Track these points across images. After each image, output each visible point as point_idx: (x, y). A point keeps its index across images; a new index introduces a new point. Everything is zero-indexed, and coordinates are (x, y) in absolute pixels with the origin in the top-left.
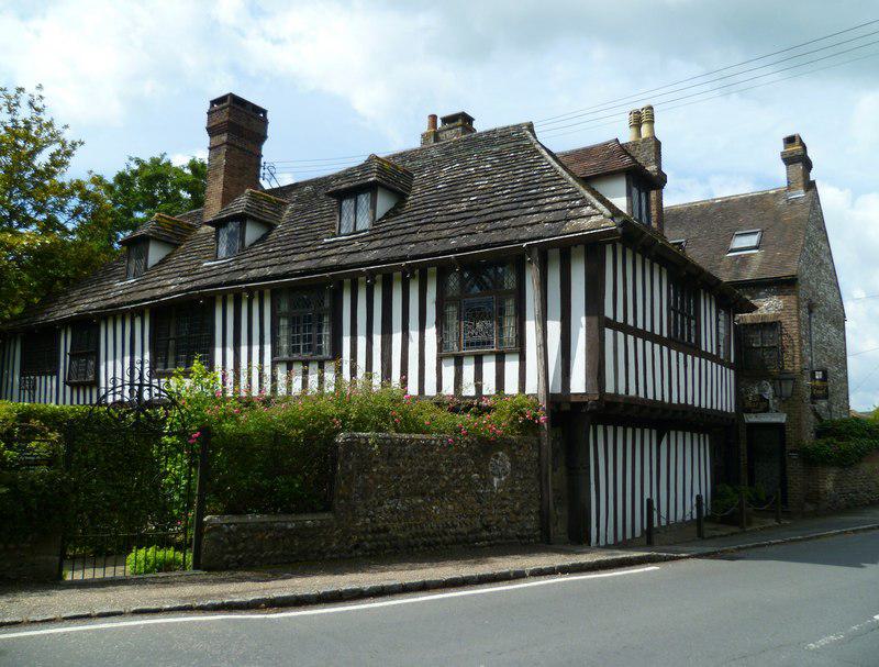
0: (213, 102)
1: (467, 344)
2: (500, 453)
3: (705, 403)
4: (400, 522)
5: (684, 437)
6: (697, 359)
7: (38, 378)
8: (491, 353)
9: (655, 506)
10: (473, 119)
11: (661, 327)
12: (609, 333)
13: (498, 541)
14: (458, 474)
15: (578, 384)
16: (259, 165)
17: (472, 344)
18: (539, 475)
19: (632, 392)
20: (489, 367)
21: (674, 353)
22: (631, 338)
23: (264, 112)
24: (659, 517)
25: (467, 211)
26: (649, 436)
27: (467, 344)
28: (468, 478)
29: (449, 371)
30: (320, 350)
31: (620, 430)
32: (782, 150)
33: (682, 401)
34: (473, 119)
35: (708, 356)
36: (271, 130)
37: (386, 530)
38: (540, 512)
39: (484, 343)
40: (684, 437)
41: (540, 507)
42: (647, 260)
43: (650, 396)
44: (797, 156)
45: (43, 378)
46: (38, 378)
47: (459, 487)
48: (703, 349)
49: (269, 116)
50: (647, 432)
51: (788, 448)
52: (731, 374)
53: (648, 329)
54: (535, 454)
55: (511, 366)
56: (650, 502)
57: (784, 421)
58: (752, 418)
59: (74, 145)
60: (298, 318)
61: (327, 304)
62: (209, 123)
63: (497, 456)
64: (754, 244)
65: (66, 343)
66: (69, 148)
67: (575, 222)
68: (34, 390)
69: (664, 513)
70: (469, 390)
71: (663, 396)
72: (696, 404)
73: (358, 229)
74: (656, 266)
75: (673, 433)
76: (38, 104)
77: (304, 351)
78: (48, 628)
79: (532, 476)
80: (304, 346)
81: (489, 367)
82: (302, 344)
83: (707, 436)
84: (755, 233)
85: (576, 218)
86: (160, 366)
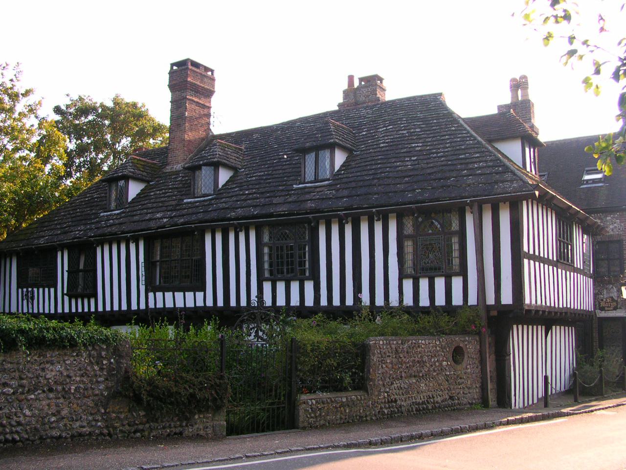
0: (173, 65)
3: (578, 306)
6: (537, 264)
7: (35, 290)
8: (441, 276)
9: (550, 381)
10: (383, 79)
11: (553, 256)
13: (458, 407)
14: (435, 362)
15: (507, 298)
19: (539, 302)
20: (440, 283)
22: (532, 262)
23: (212, 71)
24: (552, 387)
25: (412, 170)
26: (541, 330)
28: (441, 365)
29: (408, 284)
34: (383, 79)
35: (576, 270)
37: (396, 401)
39: (435, 269)
40: (542, 328)
42: (549, 209)
44: (554, 9)
45: (41, 290)
46: (35, 290)
48: (576, 266)
49: (216, 75)
50: (539, 327)
52: (591, 281)
53: (531, 252)
55: (457, 283)
56: (546, 378)
58: (603, 314)
60: (282, 248)
62: (170, 81)
65: (63, 262)
68: (33, 298)
69: (554, 386)
71: (531, 299)
72: (572, 307)
75: (554, 327)
77: (288, 272)
78: (315, 453)
79: (477, 362)
80: (288, 270)
81: (440, 283)
83: (573, 328)
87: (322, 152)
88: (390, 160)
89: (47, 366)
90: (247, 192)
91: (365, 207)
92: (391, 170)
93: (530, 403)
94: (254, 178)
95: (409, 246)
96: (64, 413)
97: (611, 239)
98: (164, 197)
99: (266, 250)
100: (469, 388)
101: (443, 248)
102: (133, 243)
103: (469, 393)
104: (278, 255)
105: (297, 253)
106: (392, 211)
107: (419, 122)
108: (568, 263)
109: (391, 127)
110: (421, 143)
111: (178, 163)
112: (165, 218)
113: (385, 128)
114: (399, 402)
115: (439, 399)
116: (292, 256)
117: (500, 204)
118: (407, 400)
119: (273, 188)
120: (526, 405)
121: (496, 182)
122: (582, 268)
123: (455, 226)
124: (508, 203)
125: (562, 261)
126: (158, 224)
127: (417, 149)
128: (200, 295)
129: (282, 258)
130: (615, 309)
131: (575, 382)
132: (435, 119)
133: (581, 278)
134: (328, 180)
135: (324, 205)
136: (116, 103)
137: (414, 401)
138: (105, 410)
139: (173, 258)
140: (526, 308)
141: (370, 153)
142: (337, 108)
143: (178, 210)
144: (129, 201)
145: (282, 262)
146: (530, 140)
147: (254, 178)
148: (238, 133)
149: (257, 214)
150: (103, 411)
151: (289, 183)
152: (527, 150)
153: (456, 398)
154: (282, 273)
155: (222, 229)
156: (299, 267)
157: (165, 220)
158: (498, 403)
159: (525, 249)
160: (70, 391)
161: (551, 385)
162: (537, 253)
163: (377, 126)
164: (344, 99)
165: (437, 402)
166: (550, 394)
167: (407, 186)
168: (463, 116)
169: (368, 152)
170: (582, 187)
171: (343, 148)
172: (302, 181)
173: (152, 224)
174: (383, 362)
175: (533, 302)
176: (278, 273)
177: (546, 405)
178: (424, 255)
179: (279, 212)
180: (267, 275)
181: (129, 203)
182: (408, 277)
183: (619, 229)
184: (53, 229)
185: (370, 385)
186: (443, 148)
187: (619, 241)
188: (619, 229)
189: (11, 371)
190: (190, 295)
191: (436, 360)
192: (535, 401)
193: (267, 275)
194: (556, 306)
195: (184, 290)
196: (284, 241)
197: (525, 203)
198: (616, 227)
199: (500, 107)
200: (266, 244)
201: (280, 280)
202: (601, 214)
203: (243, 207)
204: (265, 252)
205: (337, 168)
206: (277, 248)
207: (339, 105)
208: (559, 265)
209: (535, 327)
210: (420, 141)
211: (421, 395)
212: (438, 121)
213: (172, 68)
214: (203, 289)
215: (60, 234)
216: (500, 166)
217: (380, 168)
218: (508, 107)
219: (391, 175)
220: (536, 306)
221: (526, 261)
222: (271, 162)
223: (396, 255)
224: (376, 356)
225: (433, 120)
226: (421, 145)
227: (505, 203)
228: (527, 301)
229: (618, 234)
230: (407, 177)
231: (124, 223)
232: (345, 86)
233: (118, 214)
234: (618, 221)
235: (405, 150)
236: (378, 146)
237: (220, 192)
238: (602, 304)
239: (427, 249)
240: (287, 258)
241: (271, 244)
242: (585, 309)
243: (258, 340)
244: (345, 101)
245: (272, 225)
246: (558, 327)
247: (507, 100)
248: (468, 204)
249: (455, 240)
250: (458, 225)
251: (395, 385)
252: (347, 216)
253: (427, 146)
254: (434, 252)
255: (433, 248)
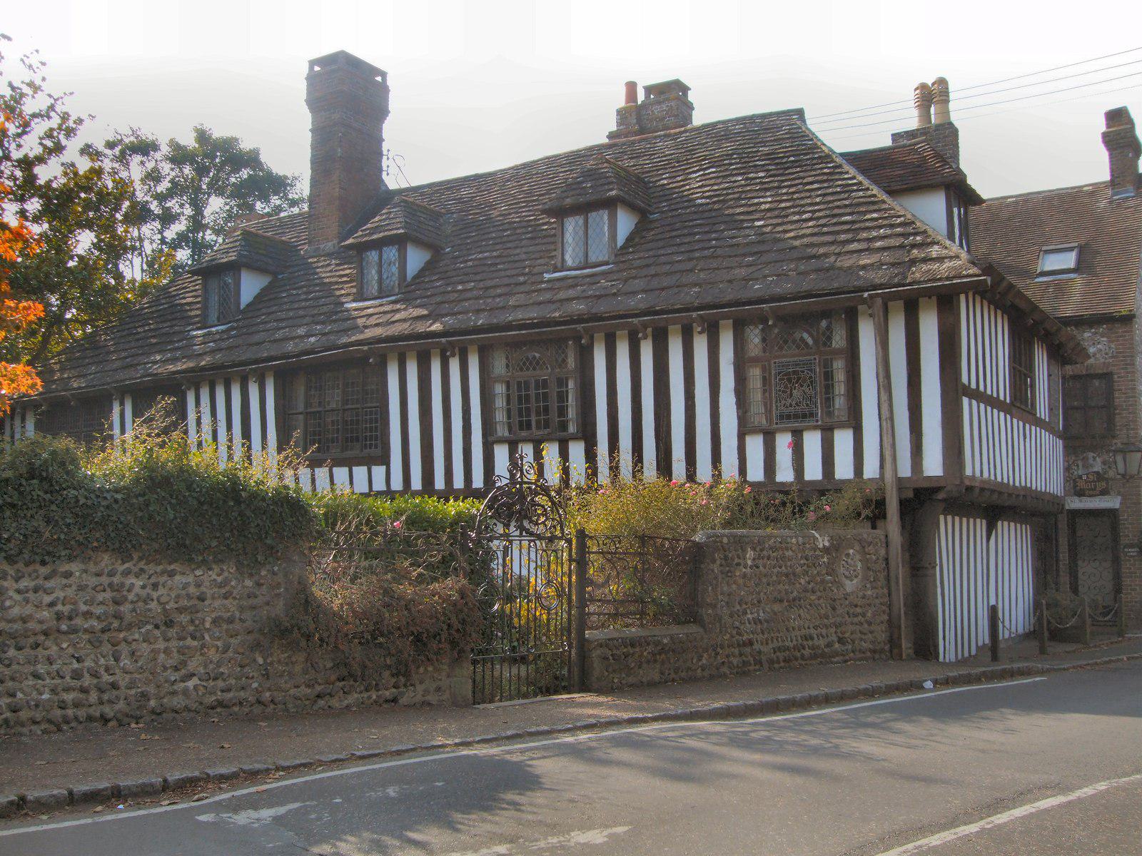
0: (312, 63)
1: (781, 417)
2: (851, 551)
4: (763, 633)
5: (1009, 526)
8: (815, 428)
12: (965, 401)
15: (933, 465)
16: (381, 154)
17: (789, 417)
18: (888, 578)
19: (986, 475)
20: (813, 442)
21: (1033, 428)
22: (974, 402)
23: (384, 75)
27: (781, 417)
29: (755, 446)
30: (563, 426)
31: (971, 520)
32: (1104, 129)
33: (1023, 484)
35: (1038, 422)
36: (394, 103)
37: (751, 643)
38: (889, 621)
39: (804, 416)
40: (1009, 526)
41: (890, 615)
43: (999, 479)
47: (813, 592)
48: (1038, 415)
51: (1124, 541)
52: (1060, 443)
54: (883, 552)
55: (843, 441)
57: (1117, 506)
58: (1075, 504)
59: (80, 121)
61: (571, 362)
63: (848, 555)
64: (1072, 265)
66: (71, 124)
67: (925, 267)
69: (1007, 624)
70: (785, 474)
71: (973, 468)
73: (593, 258)
74: (999, 313)
75: (999, 523)
76: (34, 61)
77: (538, 427)
80: (538, 422)
81: (813, 442)
82: (533, 419)
84: (1071, 249)
85: (925, 260)
86: (342, 451)
87: (594, 214)
88: (717, 227)
89: (162, 579)
90: (460, 287)
91: (678, 309)
92: (719, 243)
93: (966, 654)
94: (470, 263)
95: (755, 373)
96: (192, 665)
97: (1092, 372)
98: (306, 300)
99: (500, 389)
100: (870, 624)
101: (817, 379)
102: (255, 382)
103: (871, 632)
104: (520, 397)
105: (553, 391)
106: (726, 317)
107: (763, 160)
108: (1027, 409)
109: (714, 170)
110: (770, 196)
111: (327, 240)
112: (312, 336)
113: (702, 173)
114: (756, 646)
115: (822, 642)
116: (545, 396)
117: (921, 299)
118: (770, 642)
119: (507, 281)
120: (960, 657)
121: (913, 262)
122: (1047, 420)
123: (839, 340)
124: (934, 298)
125: (1018, 405)
126: (301, 347)
127: (763, 207)
128: (379, 471)
129: (528, 401)
130: (1104, 492)
131: (1040, 620)
132: (793, 156)
133: (1046, 436)
134: (607, 263)
135: (602, 307)
136: (202, 136)
137: (780, 644)
138: (265, 660)
139: (328, 408)
140: (967, 483)
141: (679, 215)
142: (606, 141)
143: (335, 321)
144: (242, 308)
145: (528, 409)
146: (961, 193)
147: (470, 263)
148: (430, 186)
149: (482, 325)
150: (261, 661)
151: (536, 270)
152: (955, 210)
153: (849, 641)
154: (529, 426)
155: (275, 372)
156: (559, 417)
157: (312, 339)
158: (916, 653)
159: (965, 380)
160: (204, 625)
161: (1003, 622)
162: (982, 388)
163: (686, 169)
164: (619, 124)
165: (818, 647)
166: (1001, 638)
167: (751, 271)
168: (838, 150)
169: (674, 213)
170: (1037, 280)
171: (632, 207)
172: (559, 265)
173: (290, 347)
174: (729, 574)
175: (978, 474)
176: (521, 428)
177: (995, 658)
178: (783, 392)
179: (523, 320)
180: (502, 431)
181: (242, 312)
182: (754, 431)
183: (1107, 354)
184: (101, 362)
185: (708, 614)
186: (811, 204)
187: (1106, 374)
188: (1107, 354)
189: (97, 589)
190: (360, 472)
191: (816, 572)
192: (973, 652)
193: (502, 431)
194: (1011, 483)
195: (350, 463)
196: (530, 372)
197: (962, 297)
198: (1101, 350)
199: (896, 137)
200: (499, 379)
201: (525, 440)
202: (1073, 328)
203: (455, 314)
204: (497, 392)
205: (620, 241)
206: (519, 384)
207: (611, 136)
208: (1014, 410)
209: (965, 520)
210: (768, 194)
211: (793, 635)
212: (797, 158)
213: (311, 68)
214: (385, 460)
215: (526, 260)
216: (916, 234)
217: (699, 241)
218: (911, 134)
219: (719, 252)
220: (983, 482)
221: (965, 401)
222: (500, 234)
223: (733, 393)
224: (718, 562)
225: (789, 157)
226: (770, 199)
227: (930, 297)
228: (968, 472)
229: (1104, 363)
230: (752, 254)
231: (236, 347)
232: (621, 102)
233: (223, 332)
234: (1105, 339)
235: (742, 210)
236: (691, 204)
237: (409, 289)
238: (1081, 484)
239: (789, 380)
240: (537, 400)
241: (507, 376)
242: (965, 520)
243: (521, 533)
244: (622, 127)
245: (516, 344)
246: (1006, 523)
247: (911, 122)
248: (864, 301)
249: (839, 366)
250: (845, 336)
251: (749, 616)
252: (645, 326)
253: (781, 201)
254: (802, 386)
255: (799, 379)
